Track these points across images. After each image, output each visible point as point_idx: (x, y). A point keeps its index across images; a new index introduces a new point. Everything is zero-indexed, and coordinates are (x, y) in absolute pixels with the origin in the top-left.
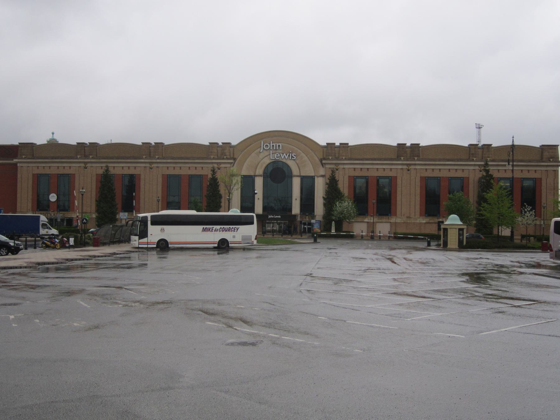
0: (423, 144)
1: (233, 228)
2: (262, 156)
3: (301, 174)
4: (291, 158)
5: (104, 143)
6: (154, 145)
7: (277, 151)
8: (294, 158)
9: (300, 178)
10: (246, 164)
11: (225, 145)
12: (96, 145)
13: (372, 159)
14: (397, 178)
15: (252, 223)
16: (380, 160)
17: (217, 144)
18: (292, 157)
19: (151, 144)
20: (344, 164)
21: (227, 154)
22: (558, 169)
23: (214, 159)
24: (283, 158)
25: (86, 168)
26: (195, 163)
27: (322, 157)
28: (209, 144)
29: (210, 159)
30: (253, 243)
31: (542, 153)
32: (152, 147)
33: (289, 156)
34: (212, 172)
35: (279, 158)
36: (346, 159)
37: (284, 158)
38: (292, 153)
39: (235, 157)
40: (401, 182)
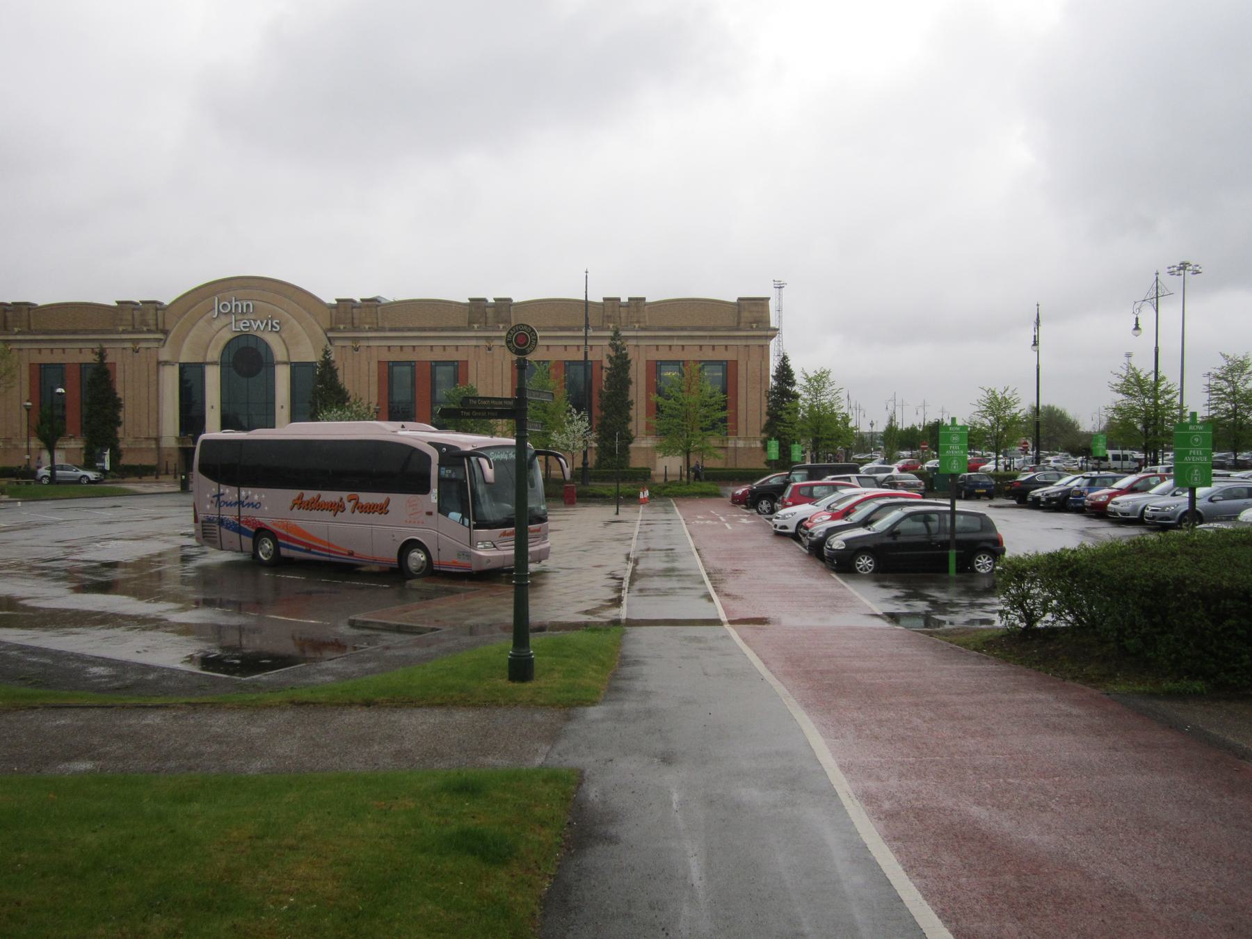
2: (217, 324)
3: (291, 357)
4: (272, 329)
7: (245, 317)
8: (276, 328)
9: (289, 366)
10: (187, 341)
11: (146, 305)
12: (377, 303)
14: (739, 362)
16: (435, 329)
17: (484, 300)
18: (272, 326)
20: (368, 338)
21: (152, 322)
22: (768, 344)
23: (124, 332)
24: (255, 329)
25: (136, 351)
27: (329, 327)
28: (469, 301)
29: (117, 333)
31: (739, 312)
32: (491, 307)
33: (267, 324)
35: (247, 330)
36: (370, 330)
37: (257, 328)
38: (272, 319)
39: (168, 327)
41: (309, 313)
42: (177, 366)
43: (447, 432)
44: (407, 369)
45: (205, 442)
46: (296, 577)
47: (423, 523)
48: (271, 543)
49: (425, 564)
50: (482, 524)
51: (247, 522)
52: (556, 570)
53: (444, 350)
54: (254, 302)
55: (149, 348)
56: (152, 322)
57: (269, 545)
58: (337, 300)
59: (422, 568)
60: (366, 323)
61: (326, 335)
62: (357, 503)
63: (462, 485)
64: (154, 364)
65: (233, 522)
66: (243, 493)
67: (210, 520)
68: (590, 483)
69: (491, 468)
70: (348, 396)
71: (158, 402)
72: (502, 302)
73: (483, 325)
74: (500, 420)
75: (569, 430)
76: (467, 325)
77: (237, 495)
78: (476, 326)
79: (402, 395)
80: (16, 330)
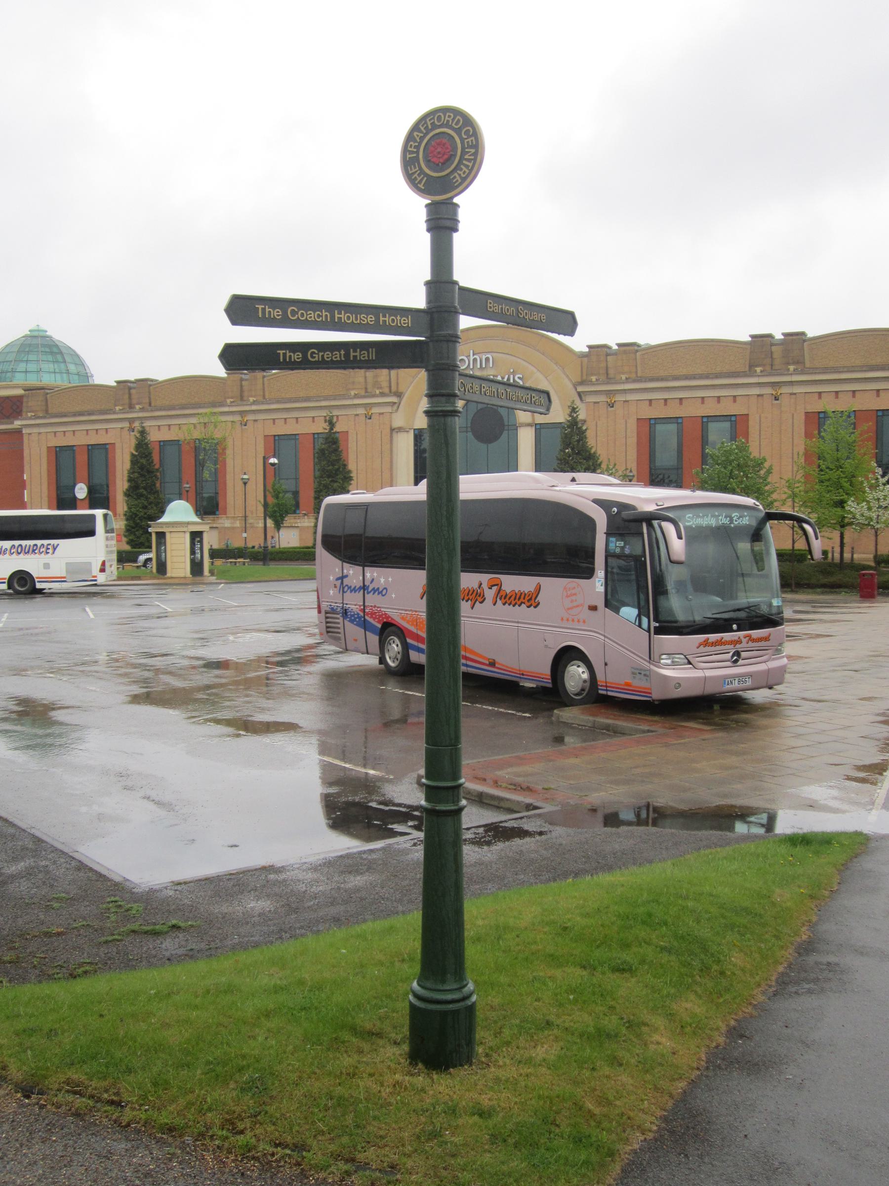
0: (812, 332)
1: (43, 545)
5: (654, 342)
6: (780, 340)
9: (534, 428)
12: (636, 348)
13: (687, 377)
15: (91, 533)
16: (707, 377)
19: (609, 347)
23: (356, 396)
26: (714, 387)
27: (580, 380)
28: (750, 339)
30: (96, 580)
34: (327, 424)
36: (628, 380)
39: (400, 390)
40: (757, 427)
41: (556, 364)
42: (412, 431)
43: (455, 444)
44: (673, 427)
45: (329, 506)
46: (417, 694)
47: (584, 622)
48: (399, 645)
49: (588, 684)
50: (667, 627)
51: (372, 614)
52: (797, 702)
53: (719, 402)
54: (494, 355)
55: (383, 414)
56: (385, 384)
57: (397, 645)
58: (590, 347)
59: (583, 690)
60: (623, 373)
61: (576, 389)
62: (499, 590)
63: (638, 562)
64: (388, 430)
65: (358, 614)
66: (368, 575)
67: (333, 611)
68: (157, 467)
69: (680, 537)
70: (599, 461)
71: (391, 474)
72: (794, 337)
73: (768, 368)
74: (385, 372)
75: (871, 496)
76: (747, 369)
77: (361, 578)
78: (758, 369)
79: (666, 458)
80: (251, 399)
